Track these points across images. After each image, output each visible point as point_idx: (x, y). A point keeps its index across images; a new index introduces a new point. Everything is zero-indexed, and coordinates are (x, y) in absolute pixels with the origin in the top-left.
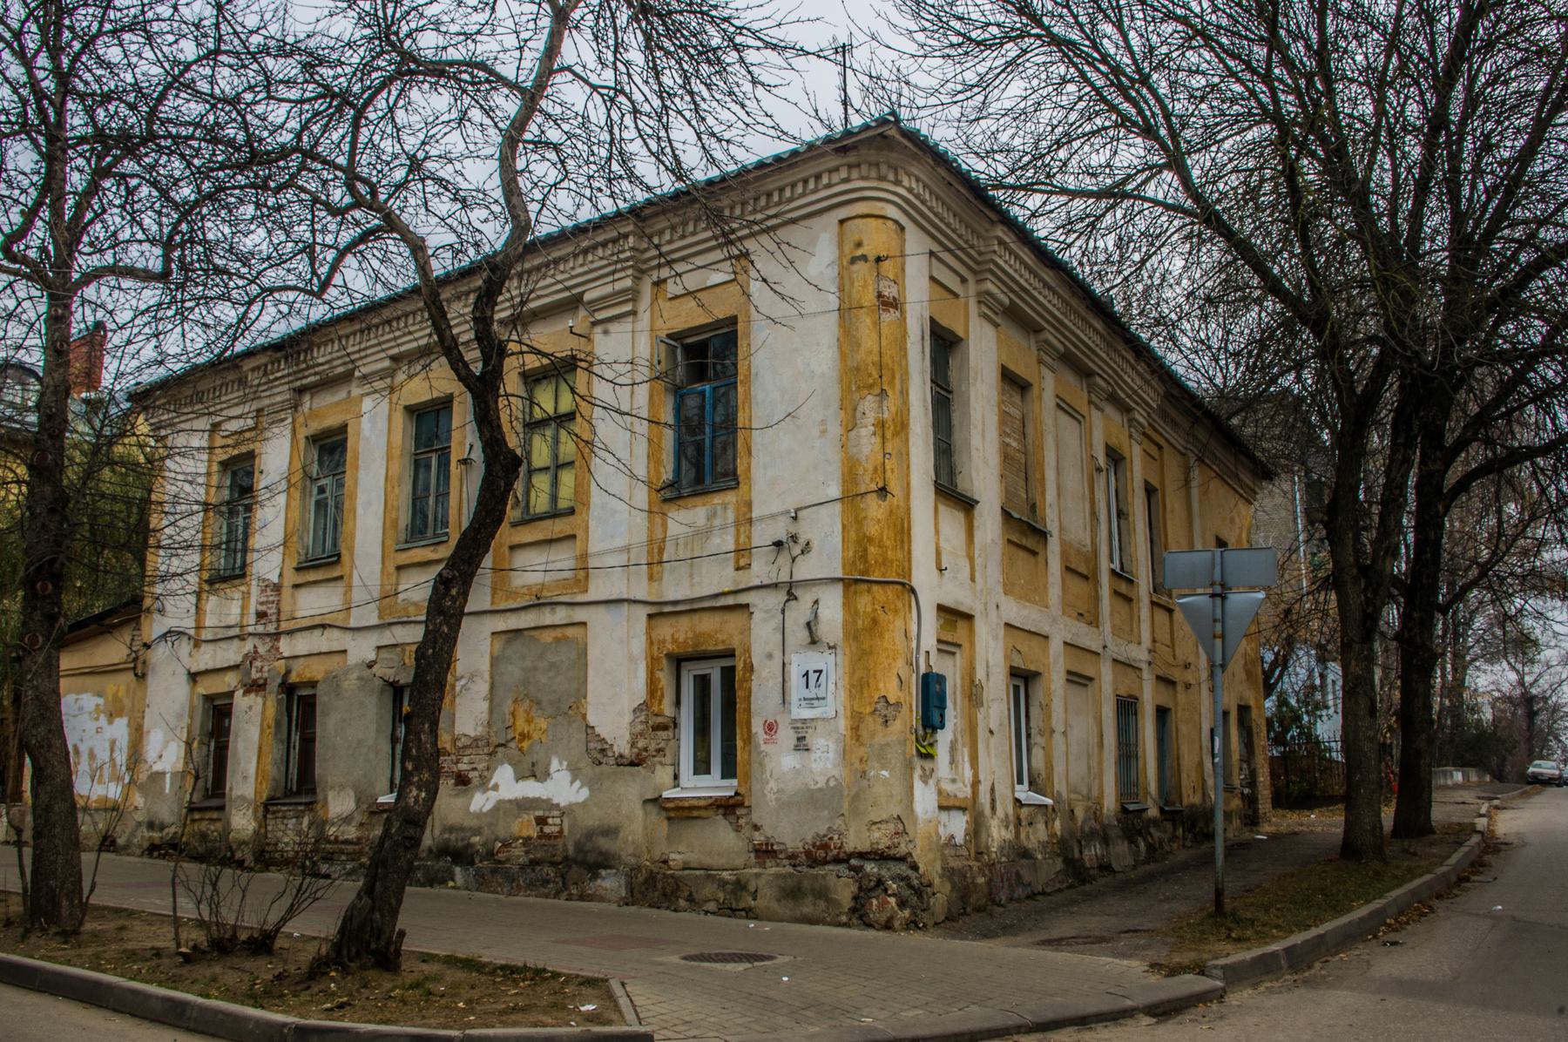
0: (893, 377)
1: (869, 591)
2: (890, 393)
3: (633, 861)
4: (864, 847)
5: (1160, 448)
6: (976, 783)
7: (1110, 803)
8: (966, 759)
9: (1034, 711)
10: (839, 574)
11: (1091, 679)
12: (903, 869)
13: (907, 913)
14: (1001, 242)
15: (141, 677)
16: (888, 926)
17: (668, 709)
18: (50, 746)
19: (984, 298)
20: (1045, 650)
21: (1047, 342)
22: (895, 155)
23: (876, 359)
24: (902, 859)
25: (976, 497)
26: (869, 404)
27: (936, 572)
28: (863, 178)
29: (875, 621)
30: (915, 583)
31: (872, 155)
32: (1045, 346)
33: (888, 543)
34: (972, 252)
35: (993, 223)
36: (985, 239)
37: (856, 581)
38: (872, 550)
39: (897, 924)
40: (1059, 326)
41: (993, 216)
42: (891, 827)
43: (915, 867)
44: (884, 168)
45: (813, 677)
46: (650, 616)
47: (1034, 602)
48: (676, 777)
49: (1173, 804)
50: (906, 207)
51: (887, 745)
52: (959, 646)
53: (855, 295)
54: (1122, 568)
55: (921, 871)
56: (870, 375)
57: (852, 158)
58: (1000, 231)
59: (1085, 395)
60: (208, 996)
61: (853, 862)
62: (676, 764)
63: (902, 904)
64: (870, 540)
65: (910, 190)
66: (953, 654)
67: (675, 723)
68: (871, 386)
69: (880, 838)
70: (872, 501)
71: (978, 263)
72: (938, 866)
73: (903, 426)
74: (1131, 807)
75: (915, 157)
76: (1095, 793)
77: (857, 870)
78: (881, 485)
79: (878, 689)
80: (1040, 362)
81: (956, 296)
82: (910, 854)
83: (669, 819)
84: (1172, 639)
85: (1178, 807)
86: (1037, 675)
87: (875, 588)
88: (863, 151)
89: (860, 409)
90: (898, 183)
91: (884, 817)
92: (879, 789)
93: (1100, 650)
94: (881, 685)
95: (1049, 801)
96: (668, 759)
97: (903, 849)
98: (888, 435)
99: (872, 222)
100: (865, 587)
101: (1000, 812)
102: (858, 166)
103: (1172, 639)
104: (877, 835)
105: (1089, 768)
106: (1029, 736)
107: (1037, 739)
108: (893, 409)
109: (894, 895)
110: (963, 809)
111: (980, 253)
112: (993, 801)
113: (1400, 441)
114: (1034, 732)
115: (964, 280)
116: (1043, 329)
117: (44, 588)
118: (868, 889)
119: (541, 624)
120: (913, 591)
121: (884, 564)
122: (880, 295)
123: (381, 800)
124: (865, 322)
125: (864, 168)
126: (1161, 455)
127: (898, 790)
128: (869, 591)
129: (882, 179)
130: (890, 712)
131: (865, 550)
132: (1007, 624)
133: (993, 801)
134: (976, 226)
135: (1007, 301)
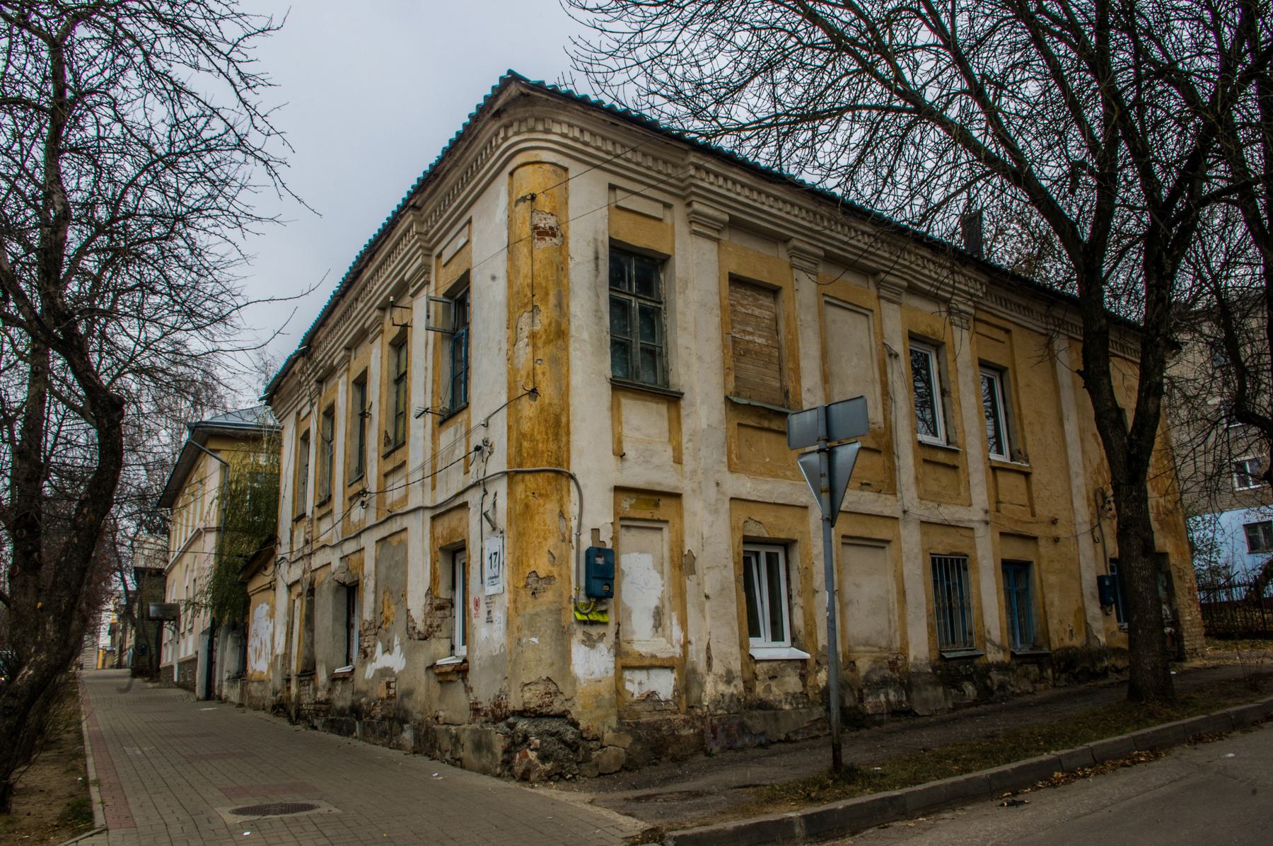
0: (547, 294)
1: (523, 481)
2: (542, 308)
3: (419, 717)
4: (519, 707)
5: (1008, 331)
6: (686, 644)
7: (919, 648)
8: (675, 621)
9: (794, 575)
10: (505, 469)
11: (888, 542)
12: (554, 725)
13: (548, 766)
14: (698, 168)
15: (274, 590)
16: (525, 778)
17: (443, 592)
18: (25, 642)
19: (694, 219)
20: (804, 520)
21: (795, 248)
22: (538, 108)
23: (530, 281)
24: (562, 716)
25: (682, 391)
26: (525, 321)
27: (612, 460)
28: (516, 134)
29: (527, 506)
30: (574, 468)
31: (520, 112)
32: (797, 252)
33: (539, 437)
34: (672, 181)
35: (686, 152)
36: (683, 167)
37: (517, 472)
38: (525, 444)
39: (533, 777)
40: (811, 234)
41: (686, 147)
42: (541, 688)
43: (575, 724)
44: (531, 122)
45: (494, 557)
46: (433, 518)
47: (786, 477)
48: (453, 648)
49: (1040, 648)
50: (565, 150)
51: (537, 614)
52: (666, 522)
53: (518, 232)
54: (948, 442)
55: (581, 727)
56: (526, 295)
57: (505, 119)
58: (693, 158)
59: (873, 290)
60: (970, 771)
61: (511, 720)
62: (451, 638)
63: (544, 758)
64: (524, 436)
65: (564, 136)
66: (661, 529)
67: (452, 603)
68: (526, 305)
69: (532, 698)
70: (525, 401)
71: (683, 189)
72: (613, 721)
73: (560, 334)
74: (947, 655)
75: (557, 107)
76: (897, 644)
77: (512, 726)
78: (530, 387)
79: (529, 566)
80: (792, 267)
81: (660, 220)
82: (569, 712)
83: (440, 682)
84: (1031, 498)
85: (1046, 650)
86: (794, 542)
87: (527, 477)
88: (511, 111)
89: (519, 326)
90: (547, 131)
91: (534, 679)
92: (529, 655)
93: (899, 514)
94: (532, 562)
95: (807, 656)
96: (444, 633)
97: (557, 707)
98: (540, 344)
99: (529, 168)
100: (520, 477)
101: (718, 667)
102: (526, 120)
103: (1031, 498)
104: (527, 695)
105: (890, 621)
106: (790, 597)
107: (797, 600)
108: (546, 322)
109: (535, 749)
110: (672, 668)
111: (682, 181)
112: (709, 659)
113: (1153, 282)
114: (794, 593)
115: (667, 206)
116: (791, 238)
117: (21, 534)
118: (517, 743)
119: (394, 531)
120: (572, 477)
121: (535, 456)
122: (536, 228)
123: (337, 671)
124: (523, 250)
125: (531, 122)
126: (1010, 338)
127: (548, 654)
128: (523, 481)
129: (532, 130)
130: (541, 585)
131: (521, 445)
132: (732, 499)
133: (709, 659)
134: (674, 160)
135: (727, 218)
